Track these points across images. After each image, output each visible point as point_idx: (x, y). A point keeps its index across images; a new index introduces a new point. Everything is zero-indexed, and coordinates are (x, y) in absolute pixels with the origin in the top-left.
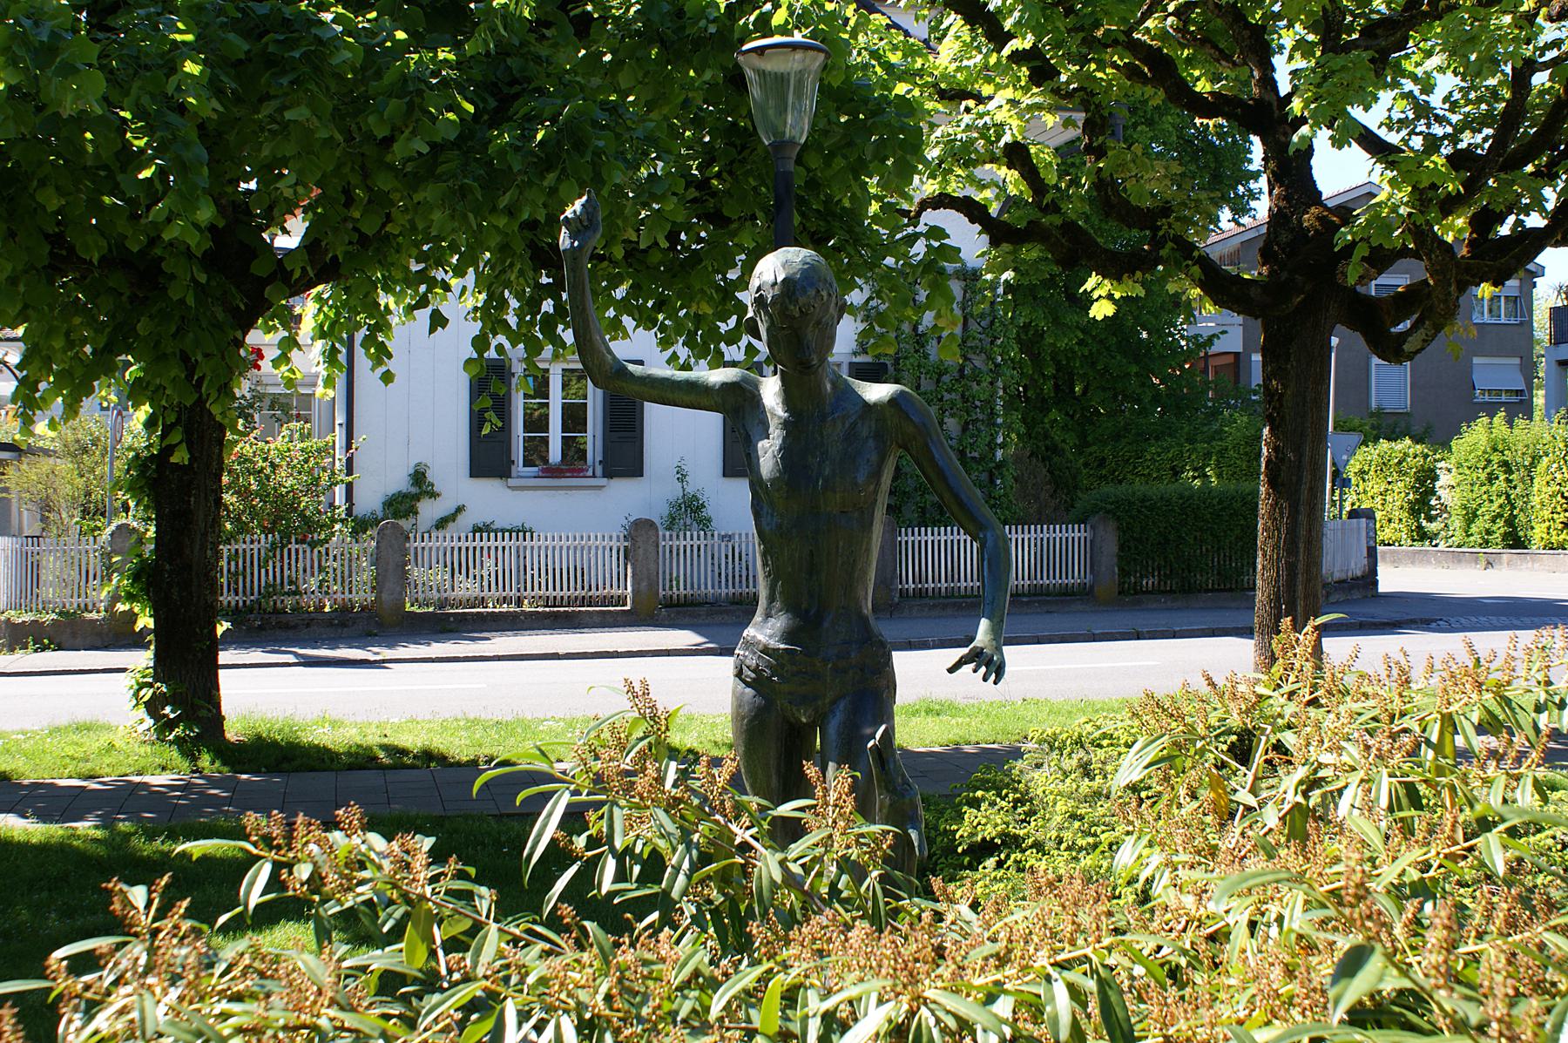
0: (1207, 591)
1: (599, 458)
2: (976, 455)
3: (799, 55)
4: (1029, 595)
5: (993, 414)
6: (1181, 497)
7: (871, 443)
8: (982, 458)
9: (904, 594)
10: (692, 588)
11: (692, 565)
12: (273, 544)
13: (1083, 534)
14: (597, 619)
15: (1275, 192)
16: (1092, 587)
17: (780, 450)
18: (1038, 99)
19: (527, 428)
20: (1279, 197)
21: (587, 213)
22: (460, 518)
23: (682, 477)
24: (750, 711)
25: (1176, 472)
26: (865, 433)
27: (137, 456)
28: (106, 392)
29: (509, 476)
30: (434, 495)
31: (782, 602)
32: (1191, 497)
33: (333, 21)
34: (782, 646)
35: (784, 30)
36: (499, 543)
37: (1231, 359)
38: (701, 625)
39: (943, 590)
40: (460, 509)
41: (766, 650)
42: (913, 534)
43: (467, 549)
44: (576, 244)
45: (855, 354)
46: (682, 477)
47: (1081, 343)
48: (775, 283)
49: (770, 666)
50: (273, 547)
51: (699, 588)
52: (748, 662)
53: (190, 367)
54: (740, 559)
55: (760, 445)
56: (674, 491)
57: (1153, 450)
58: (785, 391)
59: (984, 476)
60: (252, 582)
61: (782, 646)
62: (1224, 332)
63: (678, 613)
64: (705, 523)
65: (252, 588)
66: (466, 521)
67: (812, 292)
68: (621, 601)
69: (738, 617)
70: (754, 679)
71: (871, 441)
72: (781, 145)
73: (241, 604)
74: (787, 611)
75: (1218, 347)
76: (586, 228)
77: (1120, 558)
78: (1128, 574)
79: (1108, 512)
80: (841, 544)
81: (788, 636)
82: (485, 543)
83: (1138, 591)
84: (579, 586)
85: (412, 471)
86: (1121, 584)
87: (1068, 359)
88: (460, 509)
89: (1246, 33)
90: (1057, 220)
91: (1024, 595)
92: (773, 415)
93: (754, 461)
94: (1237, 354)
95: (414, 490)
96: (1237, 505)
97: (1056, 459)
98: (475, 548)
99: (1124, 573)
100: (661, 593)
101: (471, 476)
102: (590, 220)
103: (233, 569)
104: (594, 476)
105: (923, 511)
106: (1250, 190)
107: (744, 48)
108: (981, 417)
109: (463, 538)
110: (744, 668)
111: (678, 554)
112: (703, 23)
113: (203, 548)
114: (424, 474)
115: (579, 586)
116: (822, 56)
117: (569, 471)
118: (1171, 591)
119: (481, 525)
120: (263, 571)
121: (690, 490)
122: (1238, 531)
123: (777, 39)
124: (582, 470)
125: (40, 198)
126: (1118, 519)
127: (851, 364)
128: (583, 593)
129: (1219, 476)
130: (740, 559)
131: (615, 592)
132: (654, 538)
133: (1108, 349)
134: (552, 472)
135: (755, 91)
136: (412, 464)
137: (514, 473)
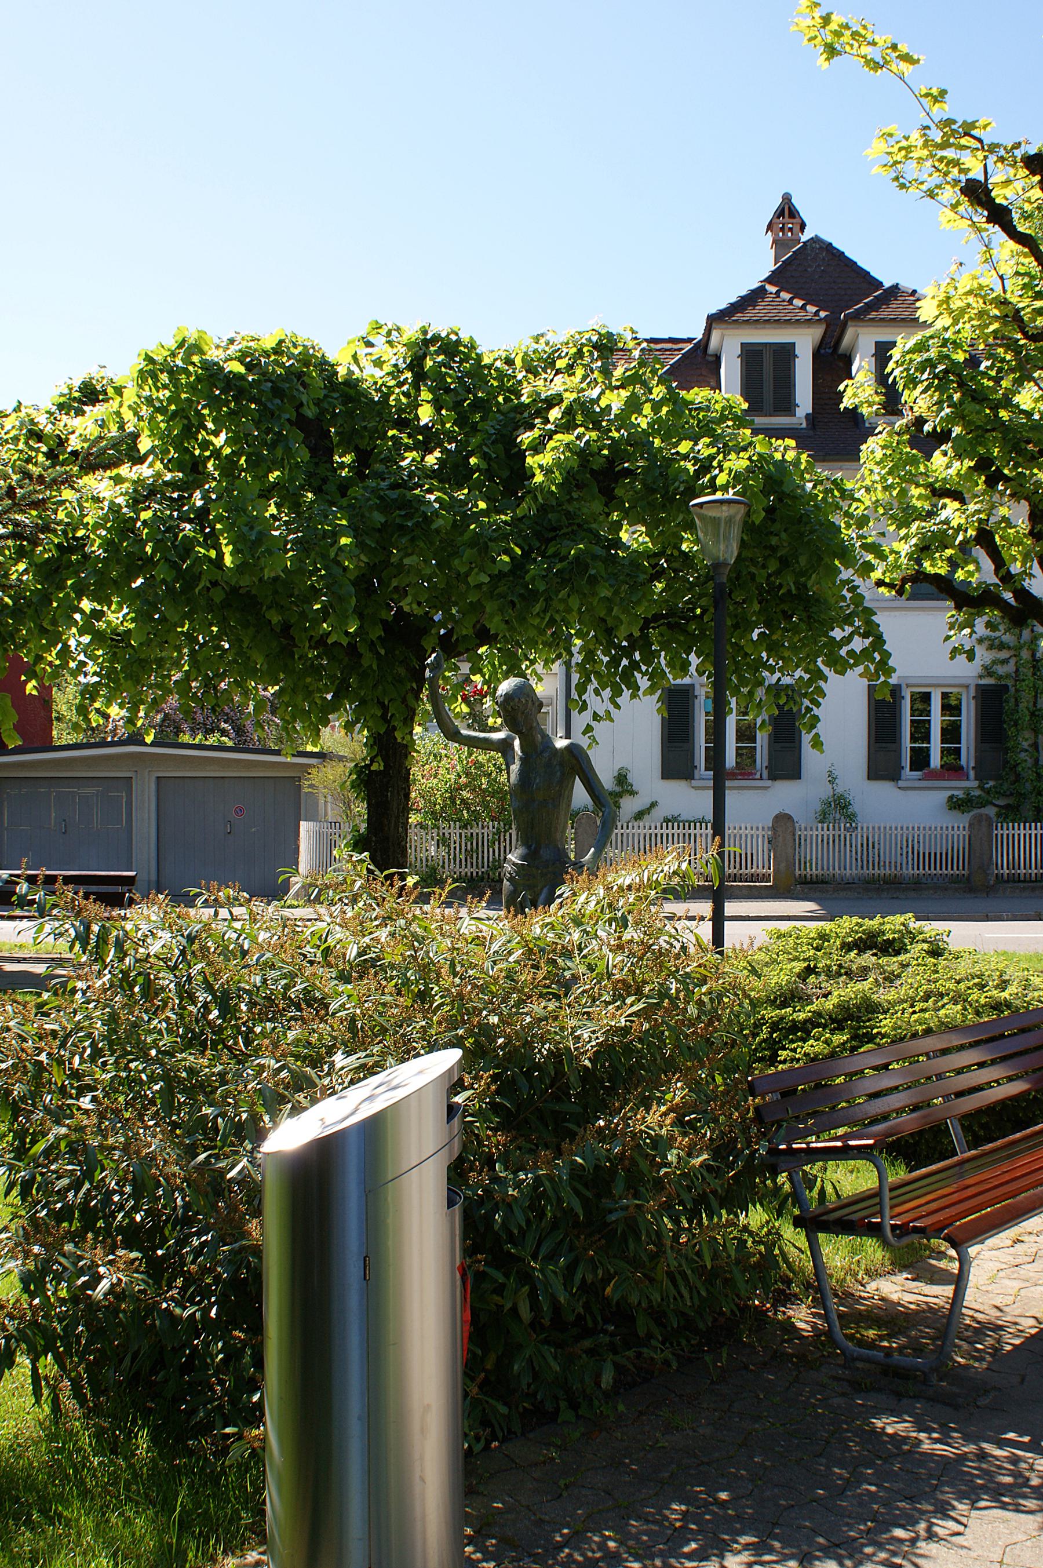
1: (765, 764)
3: (725, 508)
7: (558, 768)
10: (823, 869)
11: (839, 852)
12: (498, 829)
14: (745, 892)
19: (739, 739)
22: (653, 811)
23: (832, 780)
27: (356, 765)
28: (338, 721)
29: (693, 778)
30: (633, 793)
33: (435, 501)
35: (725, 488)
36: (698, 831)
38: (821, 899)
39: (1033, 875)
40: (653, 805)
42: (1030, 829)
43: (656, 835)
45: (980, 677)
46: (832, 780)
50: (499, 832)
51: (828, 869)
53: (385, 709)
54: (873, 847)
56: (825, 791)
60: (483, 857)
63: (810, 889)
64: (851, 817)
65: (483, 863)
66: (658, 814)
67: (517, 700)
68: (765, 878)
69: (859, 893)
73: (474, 874)
82: (670, 831)
84: (732, 866)
85: (616, 774)
88: (653, 805)
95: (618, 789)
98: (662, 835)
100: (797, 872)
101: (869, 779)
103: (469, 848)
104: (761, 778)
109: (659, 827)
111: (828, 843)
112: (676, 484)
113: (397, 827)
114: (625, 776)
115: (732, 866)
117: (741, 774)
119: (670, 817)
120: (491, 850)
121: (839, 790)
123: (719, 495)
124: (751, 774)
125: (268, 616)
127: (977, 685)
128: (735, 871)
130: (873, 847)
131: (760, 871)
132: (791, 829)
134: (934, 775)
136: (617, 768)
137: (696, 776)
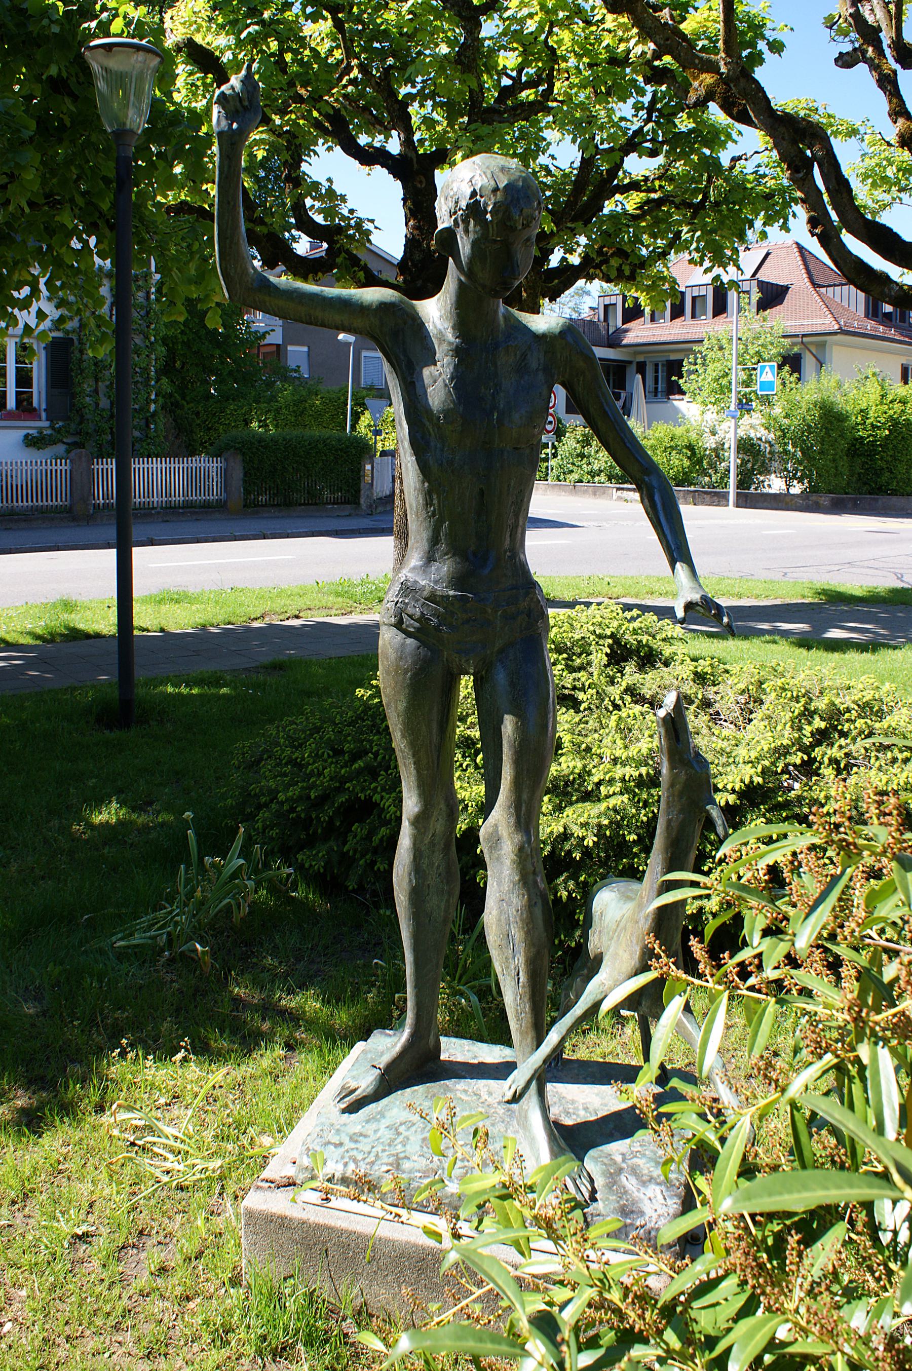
0: (300, 505)
2: (137, 407)
3: (141, 56)
4: (183, 508)
5: (148, 379)
6: (284, 439)
8: (141, 409)
9: (96, 507)
13: (219, 465)
15: (411, 223)
16: (226, 502)
17: (452, 379)
18: (264, 136)
20: (414, 227)
21: (248, 92)
24: (415, 663)
25: (247, 423)
26: (534, 365)
31: (447, 545)
32: (291, 440)
34: (451, 593)
37: (274, 348)
41: (432, 598)
44: (235, 126)
47: (182, 332)
48: (496, 190)
49: (436, 615)
52: (410, 610)
55: (426, 372)
57: (232, 407)
58: (458, 315)
59: (143, 423)
61: (451, 593)
62: (273, 330)
70: (418, 630)
71: (541, 373)
72: (122, 134)
74: (454, 555)
75: (269, 340)
76: (246, 109)
77: (245, 481)
78: (250, 493)
79: (236, 449)
80: (512, 483)
81: (458, 581)
83: (257, 505)
86: (245, 500)
87: (173, 343)
89: (396, 106)
90: (265, 230)
91: (180, 507)
92: (442, 338)
93: (419, 391)
94: (278, 346)
96: (320, 446)
97: (178, 412)
99: (247, 492)
102: (250, 101)
105: (101, 447)
106: (292, 236)
107: (92, 44)
108: (140, 379)
110: (405, 616)
112: (45, 22)
116: (158, 60)
118: (278, 505)
122: (320, 464)
126: (244, 454)
129: (276, 426)
133: (200, 338)
135: (101, 85)
